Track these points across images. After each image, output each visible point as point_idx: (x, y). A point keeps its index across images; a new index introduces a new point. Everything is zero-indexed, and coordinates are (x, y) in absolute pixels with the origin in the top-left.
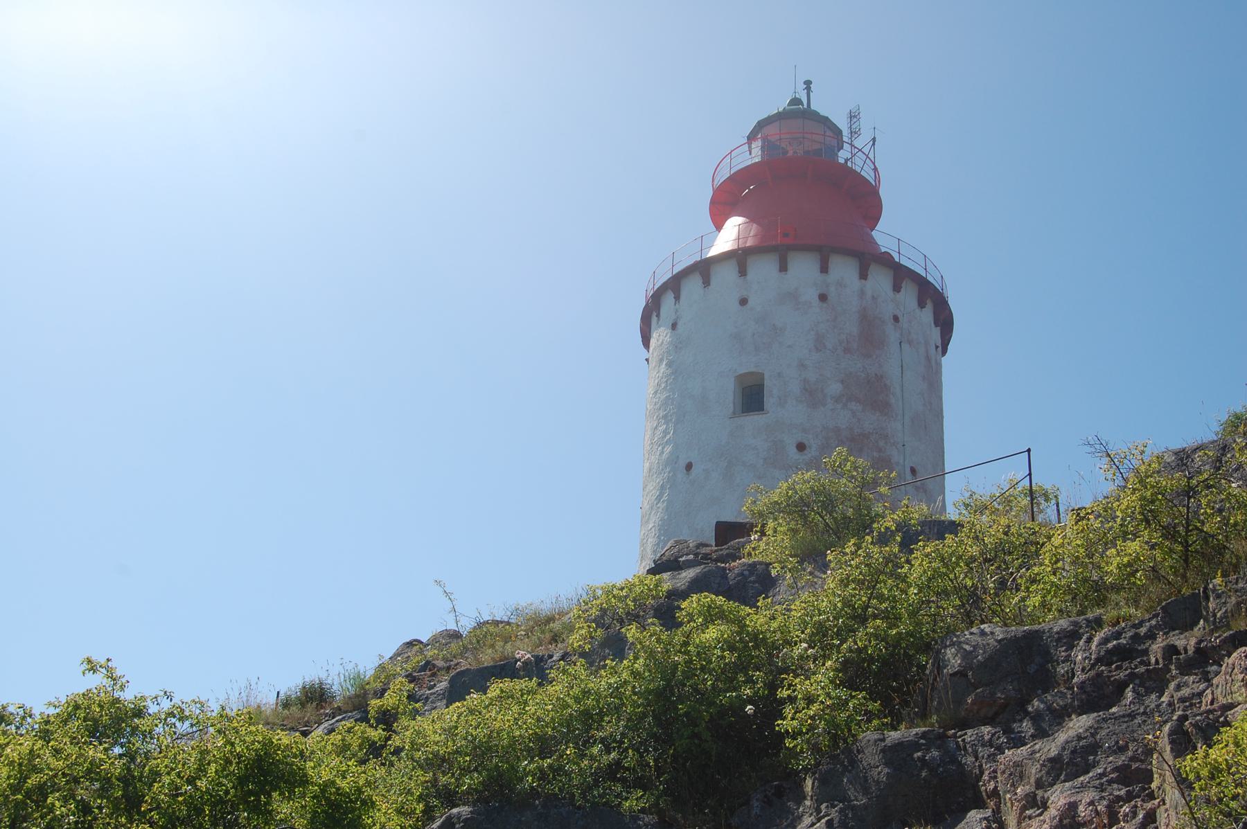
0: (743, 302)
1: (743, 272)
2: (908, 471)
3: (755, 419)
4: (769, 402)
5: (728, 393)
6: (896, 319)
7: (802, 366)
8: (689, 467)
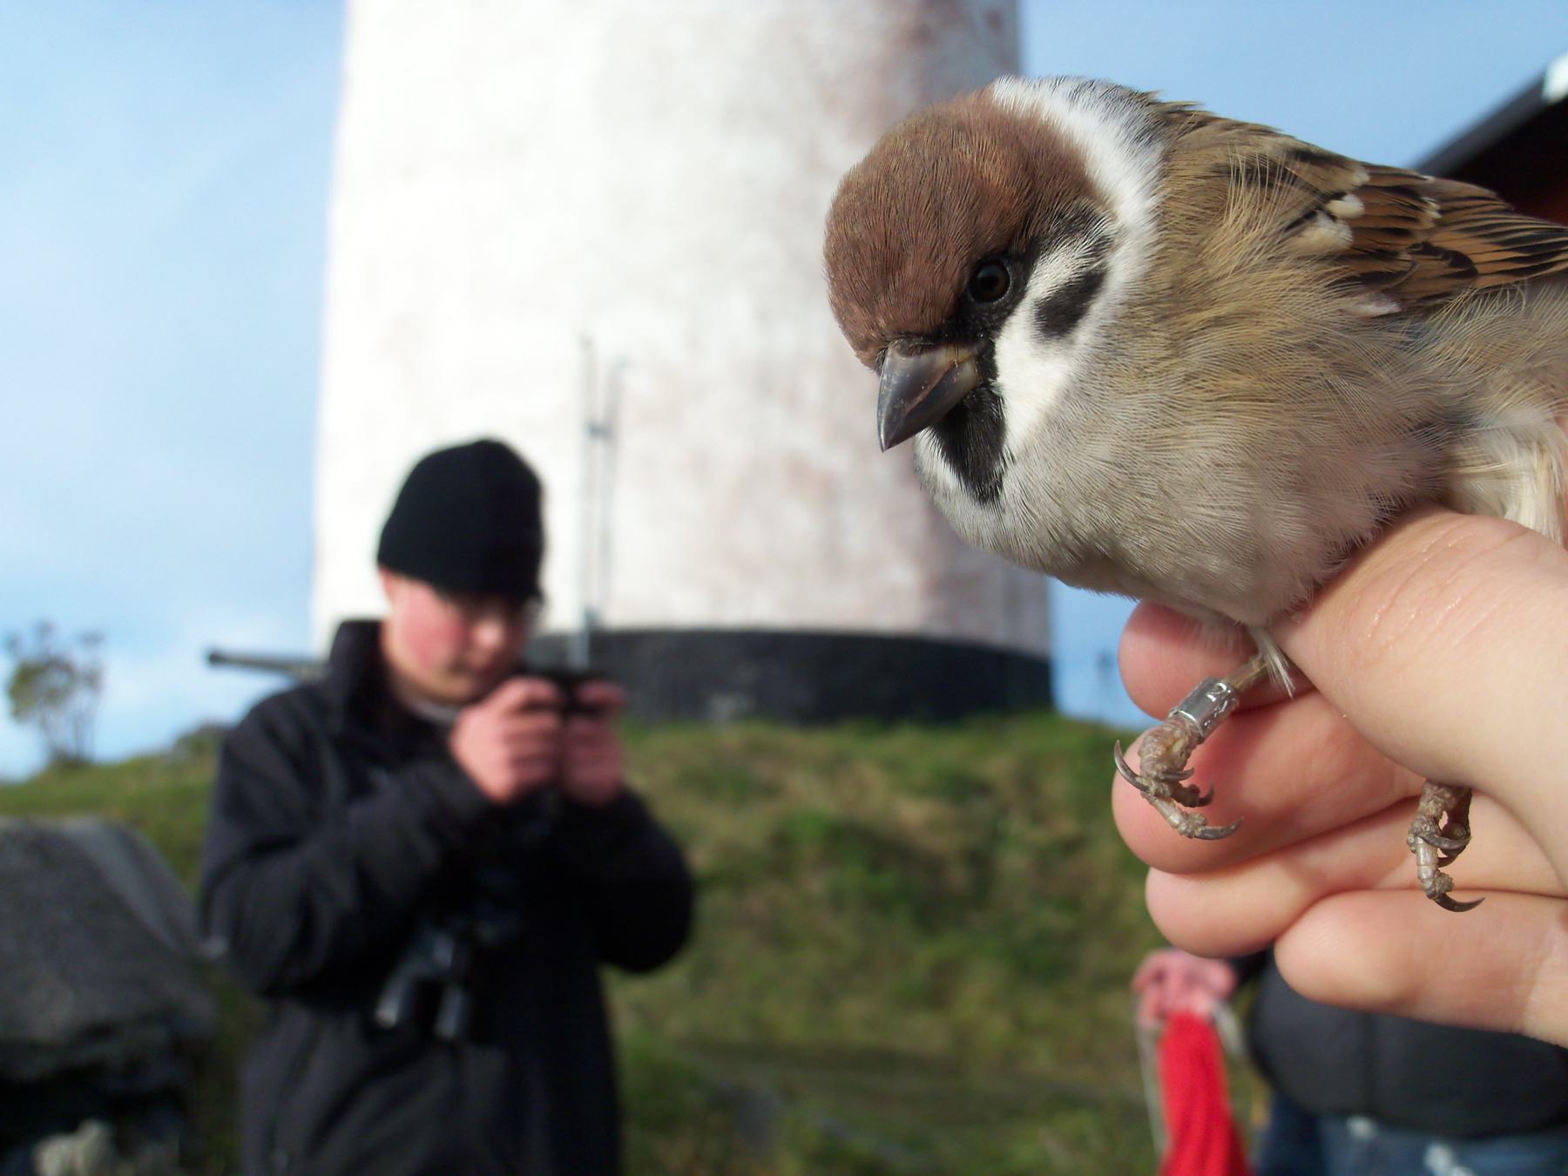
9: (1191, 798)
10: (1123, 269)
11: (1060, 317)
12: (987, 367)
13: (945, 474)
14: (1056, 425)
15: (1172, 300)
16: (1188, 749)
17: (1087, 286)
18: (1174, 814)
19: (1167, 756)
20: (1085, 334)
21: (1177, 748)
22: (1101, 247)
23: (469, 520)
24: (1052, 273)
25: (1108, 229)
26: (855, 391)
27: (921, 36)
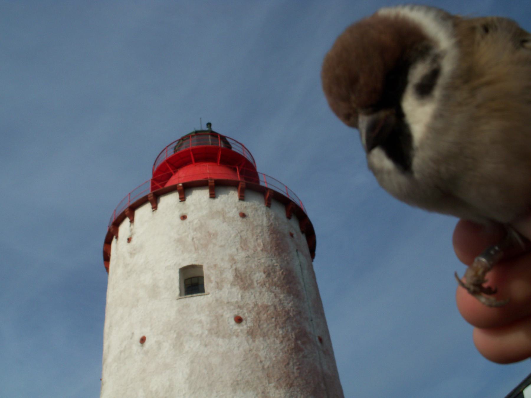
0: (184, 217)
1: (183, 199)
2: (317, 339)
3: (196, 300)
4: (208, 286)
5: (179, 220)
6: (292, 235)
7: (232, 260)
8: (143, 340)
9: (489, 291)
10: (447, 67)
11: (425, 90)
12: (400, 115)
13: (387, 164)
14: (435, 130)
15: (468, 75)
16: (484, 273)
17: (435, 74)
18: (483, 299)
19: (476, 275)
20: (437, 92)
21: (480, 272)
22: (437, 58)
23: (209, 125)
24: (418, 72)
25: (436, 51)
26: (354, 138)
27: (297, 349)
